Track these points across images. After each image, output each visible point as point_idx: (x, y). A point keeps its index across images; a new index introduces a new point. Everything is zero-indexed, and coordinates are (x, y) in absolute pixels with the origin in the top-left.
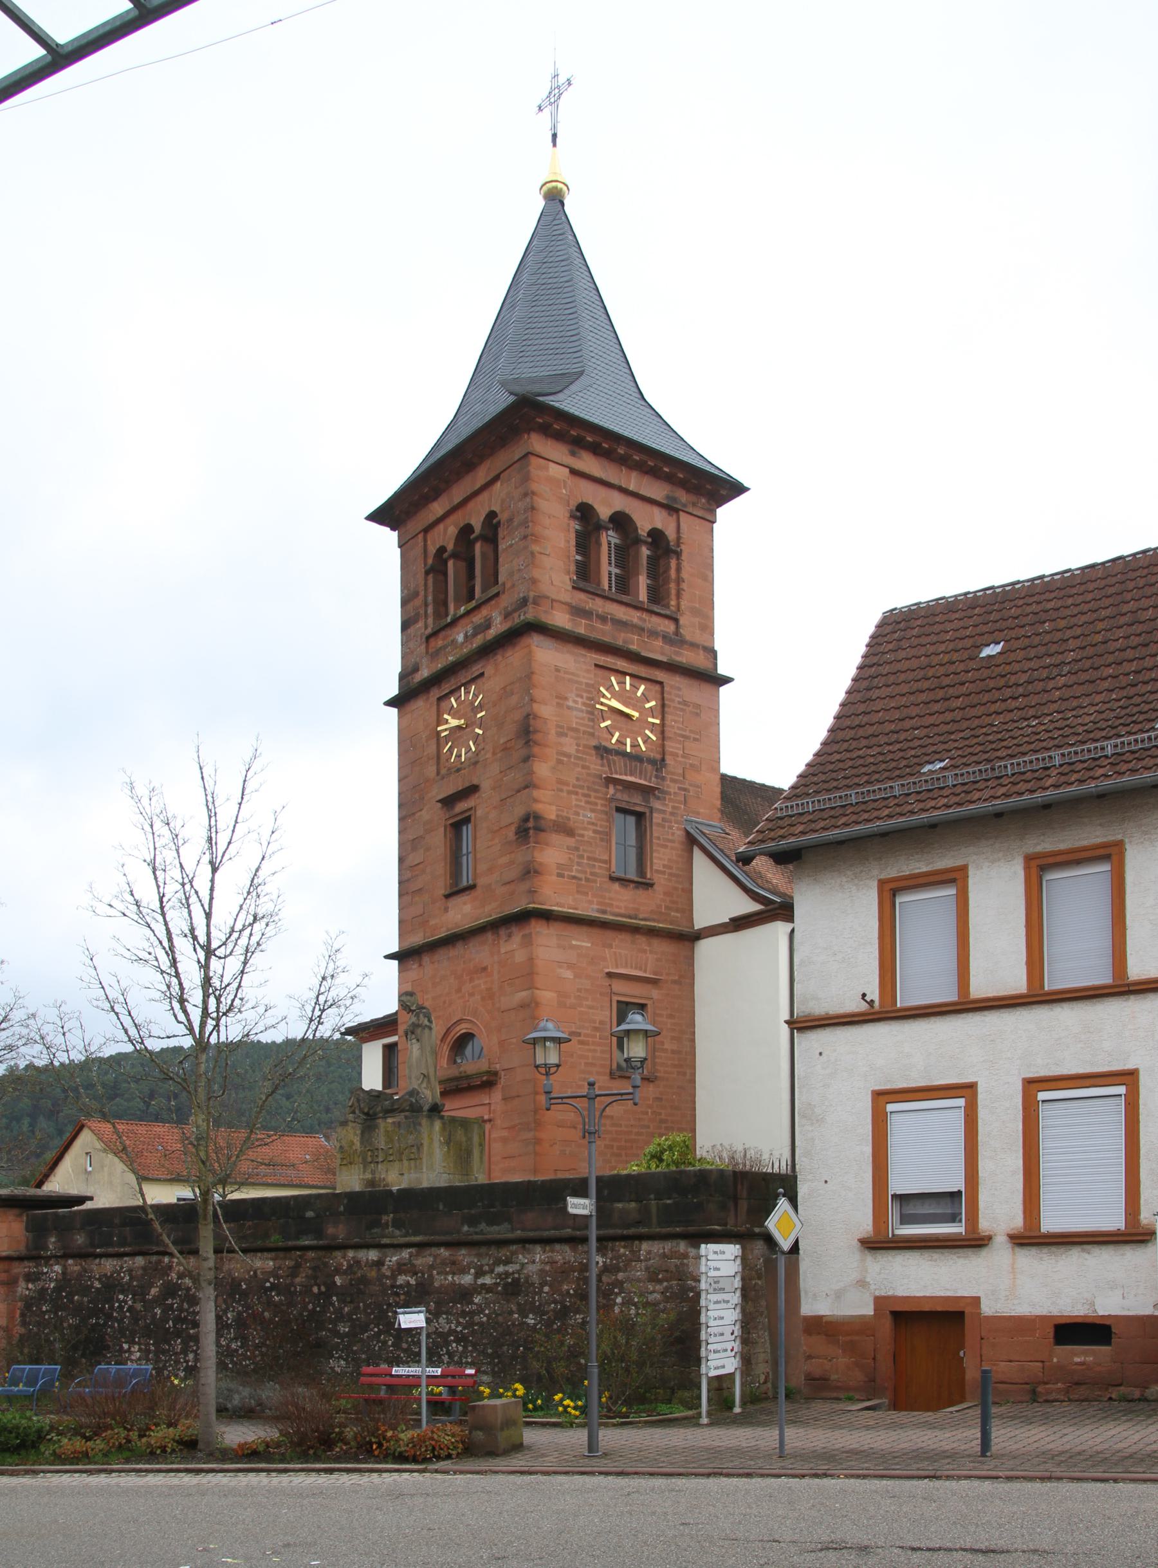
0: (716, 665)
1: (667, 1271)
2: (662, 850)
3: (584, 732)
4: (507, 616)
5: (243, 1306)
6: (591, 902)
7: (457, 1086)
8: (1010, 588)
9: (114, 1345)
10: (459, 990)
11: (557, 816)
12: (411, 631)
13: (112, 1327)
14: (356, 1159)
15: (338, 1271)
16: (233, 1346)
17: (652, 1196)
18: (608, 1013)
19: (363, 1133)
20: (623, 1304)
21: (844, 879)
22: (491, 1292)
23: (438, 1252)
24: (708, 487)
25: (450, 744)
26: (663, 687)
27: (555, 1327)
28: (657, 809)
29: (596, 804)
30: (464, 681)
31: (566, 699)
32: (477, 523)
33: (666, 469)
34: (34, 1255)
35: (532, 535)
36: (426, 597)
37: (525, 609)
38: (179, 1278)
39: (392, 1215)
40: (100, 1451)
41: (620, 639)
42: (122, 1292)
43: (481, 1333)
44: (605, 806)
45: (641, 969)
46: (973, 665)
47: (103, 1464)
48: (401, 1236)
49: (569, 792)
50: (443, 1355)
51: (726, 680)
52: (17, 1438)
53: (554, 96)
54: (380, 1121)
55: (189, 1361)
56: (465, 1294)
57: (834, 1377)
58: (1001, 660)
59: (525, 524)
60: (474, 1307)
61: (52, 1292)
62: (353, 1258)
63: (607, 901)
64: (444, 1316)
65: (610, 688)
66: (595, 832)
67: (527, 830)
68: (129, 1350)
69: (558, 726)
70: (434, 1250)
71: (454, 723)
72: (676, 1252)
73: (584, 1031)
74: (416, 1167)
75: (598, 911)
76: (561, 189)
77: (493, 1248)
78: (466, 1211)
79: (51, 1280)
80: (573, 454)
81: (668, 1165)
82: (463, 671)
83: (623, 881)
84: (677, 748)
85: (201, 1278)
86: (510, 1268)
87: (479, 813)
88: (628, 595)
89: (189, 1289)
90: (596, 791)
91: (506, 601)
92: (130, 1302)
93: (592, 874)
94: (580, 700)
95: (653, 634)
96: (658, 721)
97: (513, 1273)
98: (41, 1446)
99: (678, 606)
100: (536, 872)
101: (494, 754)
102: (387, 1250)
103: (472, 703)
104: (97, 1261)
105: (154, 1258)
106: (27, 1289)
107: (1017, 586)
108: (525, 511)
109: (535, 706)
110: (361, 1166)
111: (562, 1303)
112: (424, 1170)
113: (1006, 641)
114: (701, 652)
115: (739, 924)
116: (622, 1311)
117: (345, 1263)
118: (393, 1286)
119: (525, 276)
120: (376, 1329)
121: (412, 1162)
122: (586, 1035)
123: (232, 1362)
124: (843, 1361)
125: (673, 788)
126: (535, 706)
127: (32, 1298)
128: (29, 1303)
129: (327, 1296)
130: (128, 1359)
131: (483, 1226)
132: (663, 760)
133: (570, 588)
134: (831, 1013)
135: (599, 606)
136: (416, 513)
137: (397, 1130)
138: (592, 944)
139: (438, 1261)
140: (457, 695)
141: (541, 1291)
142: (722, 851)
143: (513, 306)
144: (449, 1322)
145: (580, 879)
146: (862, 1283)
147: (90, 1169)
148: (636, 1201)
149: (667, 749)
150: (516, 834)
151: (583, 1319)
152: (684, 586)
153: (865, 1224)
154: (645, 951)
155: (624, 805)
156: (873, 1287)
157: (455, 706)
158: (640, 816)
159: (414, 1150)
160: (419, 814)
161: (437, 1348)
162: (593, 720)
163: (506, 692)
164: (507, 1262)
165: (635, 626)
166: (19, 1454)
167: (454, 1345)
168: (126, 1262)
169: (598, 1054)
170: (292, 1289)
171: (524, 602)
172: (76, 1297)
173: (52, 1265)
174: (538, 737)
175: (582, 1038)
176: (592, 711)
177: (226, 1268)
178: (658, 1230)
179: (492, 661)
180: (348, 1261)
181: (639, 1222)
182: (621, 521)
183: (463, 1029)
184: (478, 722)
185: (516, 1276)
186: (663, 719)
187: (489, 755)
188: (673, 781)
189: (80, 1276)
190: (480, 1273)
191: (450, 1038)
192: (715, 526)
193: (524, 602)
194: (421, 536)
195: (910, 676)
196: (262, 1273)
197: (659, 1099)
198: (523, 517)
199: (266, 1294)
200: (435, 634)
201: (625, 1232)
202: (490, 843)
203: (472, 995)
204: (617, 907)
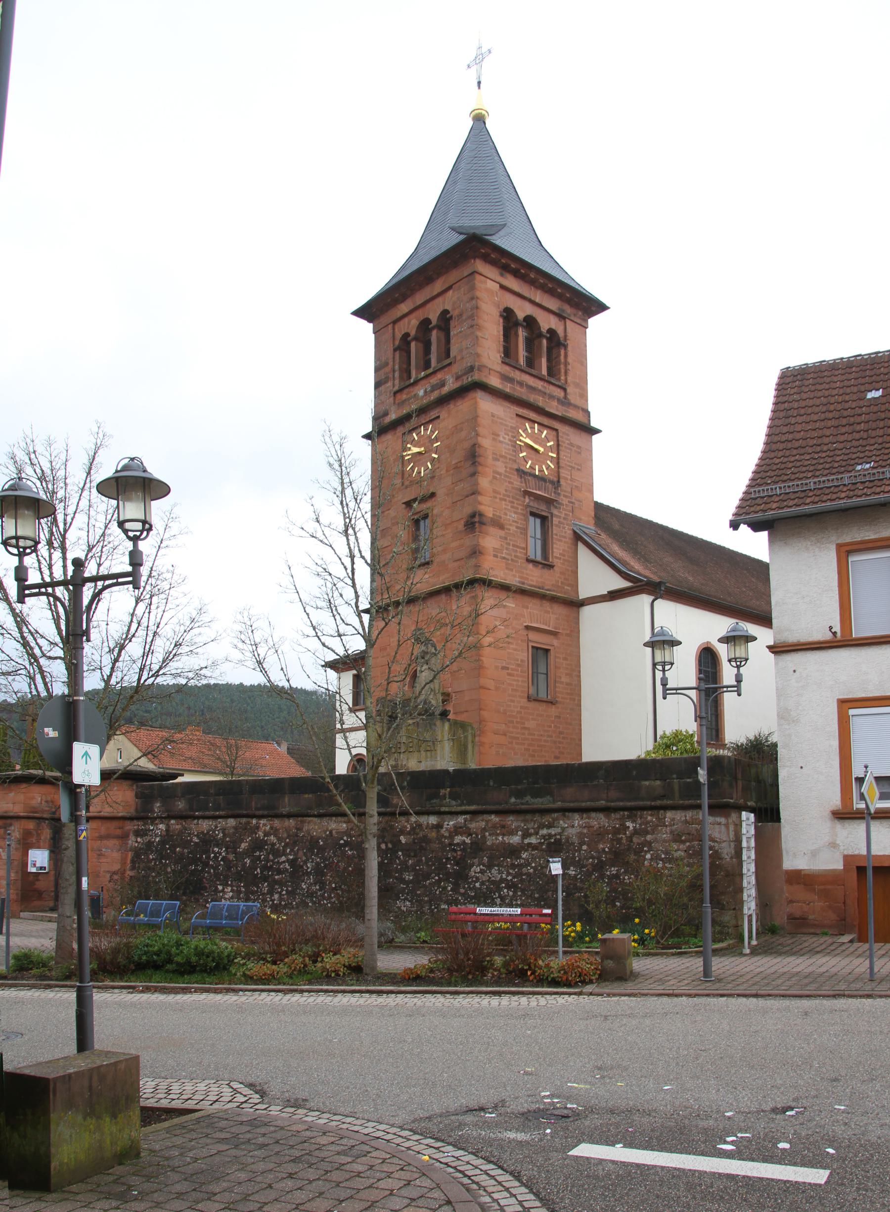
0: (590, 421)
1: (689, 834)
2: (559, 543)
3: (510, 459)
4: (458, 378)
5: (321, 858)
6: (514, 576)
8: (874, 355)
11: (493, 515)
12: (382, 388)
13: (209, 872)
15: (402, 832)
17: (675, 776)
18: (526, 654)
20: (651, 859)
21: (809, 543)
22: (536, 849)
23: (490, 818)
24: (584, 304)
27: (594, 877)
28: (556, 515)
29: (518, 508)
30: (424, 422)
31: (498, 435)
32: (434, 318)
33: (559, 290)
34: (142, 815)
35: (477, 325)
36: (394, 366)
37: (473, 373)
38: (265, 836)
39: (448, 789)
40: (285, 973)
41: (532, 398)
42: (217, 845)
43: (529, 881)
44: (523, 510)
45: (546, 625)
46: (861, 403)
47: (292, 985)
49: (501, 499)
50: (496, 898)
51: (596, 431)
52: (213, 961)
53: (479, 59)
55: (274, 900)
56: (513, 851)
57: (811, 917)
58: (884, 400)
59: (472, 317)
60: (522, 861)
61: (158, 845)
62: (415, 822)
63: (525, 576)
64: (496, 868)
65: (525, 430)
66: (517, 527)
67: (473, 524)
68: (223, 891)
69: (494, 454)
70: (486, 817)
71: (415, 450)
72: (696, 819)
73: (511, 667)
74: (431, 756)
75: (520, 582)
76: (484, 115)
77: (537, 815)
78: (513, 786)
79: (156, 835)
80: (502, 275)
81: (681, 753)
83: (534, 562)
84: (568, 475)
85: (368, 832)
86: (553, 831)
87: (435, 512)
88: (534, 369)
89: (273, 844)
90: (517, 499)
91: (456, 369)
92: (223, 854)
93: (516, 556)
94: (507, 437)
95: (551, 397)
96: (555, 455)
97: (555, 835)
98: (231, 969)
99: (566, 380)
100: (480, 552)
101: (447, 471)
103: (430, 436)
104: (196, 821)
105: (244, 820)
106: (137, 842)
107: (880, 355)
108: (472, 309)
109: (479, 438)
111: (599, 858)
112: (439, 759)
113: (883, 389)
114: (581, 412)
115: (614, 595)
116: (651, 865)
117: (409, 826)
118: (450, 844)
119: (463, 165)
120: (437, 878)
121: (429, 753)
122: (513, 670)
123: (312, 901)
124: (819, 904)
125: (565, 501)
126: (479, 438)
127: (140, 849)
128: (137, 853)
129: (394, 851)
130: (222, 897)
131: (528, 798)
132: (559, 482)
133: (500, 362)
134: (802, 641)
135: (517, 375)
136: (387, 311)
138: (516, 605)
139: (490, 825)
140: (418, 431)
141: (580, 850)
142: (600, 545)
143: (455, 183)
144: (500, 872)
145: (508, 560)
146: (833, 845)
147: (120, 760)
148: (660, 780)
149: (562, 475)
150: (465, 526)
151: (617, 870)
152: (569, 367)
153: (835, 800)
154: (548, 612)
155: (534, 510)
156: (842, 848)
157: (416, 438)
158: (544, 519)
159: (430, 744)
160: (388, 512)
161: (491, 893)
162: (515, 451)
164: (550, 826)
165: (540, 391)
166: (214, 975)
167: (505, 891)
168: (220, 823)
169: (520, 683)
171: (471, 369)
172: (178, 849)
173: (157, 824)
174: (480, 460)
175: (510, 671)
176: (514, 445)
177: (305, 828)
178: (681, 802)
179: (446, 408)
180: (411, 825)
181: (664, 796)
182: (530, 322)
184: (435, 450)
185: (558, 837)
186: (558, 454)
187: (443, 472)
188: (565, 496)
189: (181, 833)
190: (526, 835)
192: (587, 330)
193: (471, 369)
194: (390, 326)
195: (817, 409)
196: (337, 833)
197: (559, 717)
200: (400, 390)
201: (653, 804)
204: (532, 580)
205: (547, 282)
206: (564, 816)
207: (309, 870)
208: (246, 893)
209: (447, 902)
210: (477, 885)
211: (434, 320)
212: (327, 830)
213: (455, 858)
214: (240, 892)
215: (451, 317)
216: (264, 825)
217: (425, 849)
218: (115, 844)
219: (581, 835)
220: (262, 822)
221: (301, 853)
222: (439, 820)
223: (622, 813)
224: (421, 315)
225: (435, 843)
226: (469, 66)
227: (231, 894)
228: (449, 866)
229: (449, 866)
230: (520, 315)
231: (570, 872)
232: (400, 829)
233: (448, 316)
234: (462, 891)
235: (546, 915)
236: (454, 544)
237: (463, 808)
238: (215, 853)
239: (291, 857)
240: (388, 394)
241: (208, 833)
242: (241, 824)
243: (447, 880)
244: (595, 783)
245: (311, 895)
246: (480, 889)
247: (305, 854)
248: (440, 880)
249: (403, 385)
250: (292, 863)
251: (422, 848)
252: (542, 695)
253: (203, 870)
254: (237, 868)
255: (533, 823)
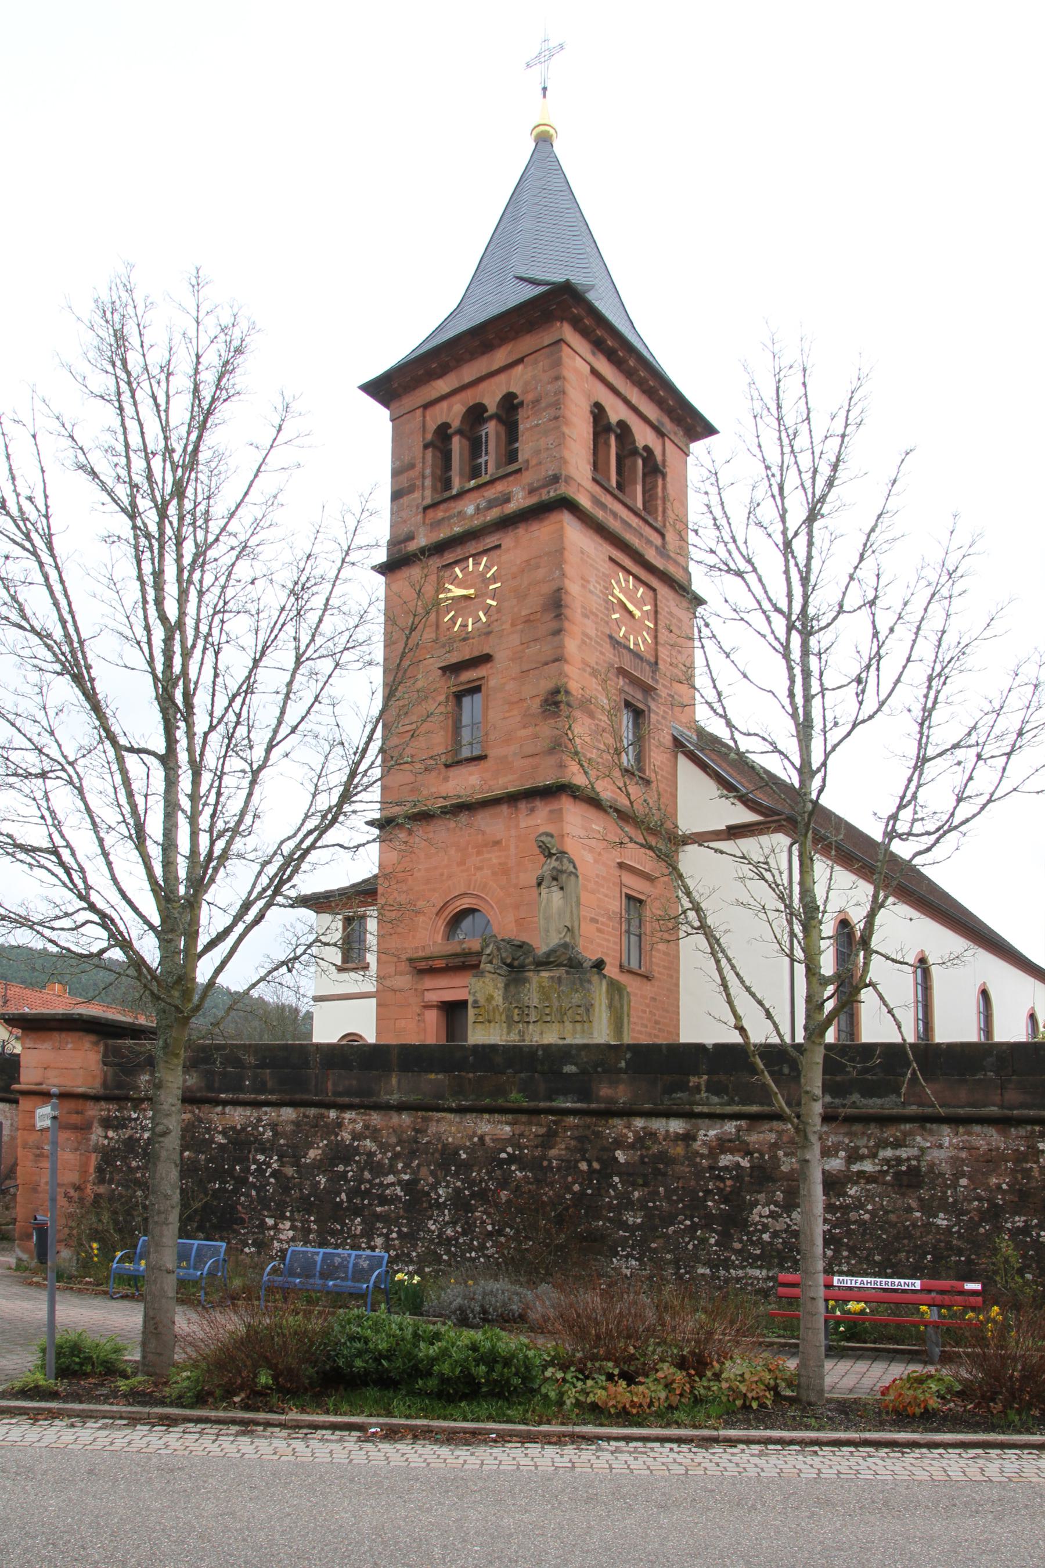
4: (532, 491)
5: (463, 1181)
7: (463, 963)
9: (251, 1219)
10: (462, 863)
12: (405, 500)
13: (248, 1195)
14: (497, 1017)
16: (449, 1232)
18: (618, 904)
19: (507, 986)
23: (784, 1127)
25: (453, 613)
26: (656, 595)
27: (982, 1230)
30: (474, 552)
32: (492, 404)
36: (423, 469)
38: (353, 1139)
39: (705, 1077)
42: (263, 1151)
43: (864, 1234)
48: (721, 1105)
53: (545, 55)
54: (531, 974)
60: (849, 1201)
62: (644, 1128)
65: (618, 582)
67: (557, 704)
68: (275, 1227)
71: (458, 592)
73: (601, 919)
74: (583, 1032)
77: (872, 1126)
79: (144, 1129)
80: (594, 354)
82: (473, 542)
86: (904, 1153)
87: (492, 683)
89: (371, 1154)
91: (528, 478)
95: (649, 542)
97: (909, 1159)
101: (513, 625)
102: (700, 1121)
104: (219, 1109)
105: (312, 1112)
106: (106, 1137)
108: (555, 393)
110: (505, 1025)
117: (631, 1134)
118: (711, 1168)
120: (688, 1223)
121: (578, 1026)
122: (603, 924)
123: (448, 1252)
127: (113, 1149)
128: (108, 1156)
129: (604, 1175)
130: (273, 1238)
132: (656, 663)
136: (415, 388)
137: (556, 986)
139: (785, 1139)
140: (464, 565)
141: (955, 1185)
149: (660, 655)
151: (1025, 1222)
157: (460, 575)
163: (529, 565)
164: (897, 1145)
165: (635, 529)
168: (266, 1113)
170: (545, 1163)
173: (145, 1110)
174: (567, 612)
177: (433, 1129)
180: (636, 1133)
182: (624, 431)
183: (465, 903)
185: (914, 1163)
186: (656, 624)
187: (507, 626)
190: (854, 1156)
191: (446, 912)
193: (555, 479)
194: (419, 412)
196: (494, 1140)
197: (653, 999)
198: (554, 399)
199: (501, 1168)
200: (434, 505)
202: (507, 715)
203: (480, 868)
205: (648, 376)
206: (924, 1129)
207: (441, 1200)
208: (320, 1233)
209: (708, 1263)
210: (766, 1237)
211: (492, 407)
212: (474, 1134)
213: (720, 1191)
214: (309, 1231)
215: (521, 404)
216: (352, 1121)
217: (665, 1174)
218: (68, 1139)
219: (954, 1160)
220: (348, 1115)
221: (424, 1171)
222: (688, 1127)
223: (1029, 1128)
224: (469, 398)
225: (682, 1164)
226: (528, 65)
227: (291, 1233)
228: (710, 1203)
229: (710, 1203)
230: (614, 419)
231: (939, 1222)
232: (615, 1139)
233: (515, 401)
234: (737, 1246)
235: (974, 1293)
236: (523, 733)
237: (736, 1109)
238: (259, 1164)
239: (407, 1177)
240: (414, 509)
241: (244, 1129)
242: (308, 1117)
243: (707, 1227)
244: (980, 1076)
245: (446, 1242)
246: (770, 1243)
247: (433, 1173)
248: (694, 1227)
249: (438, 498)
250: (409, 1187)
251: (657, 1172)
252: (634, 965)
253: (236, 1191)
254: (301, 1190)
255: (865, 1139)
